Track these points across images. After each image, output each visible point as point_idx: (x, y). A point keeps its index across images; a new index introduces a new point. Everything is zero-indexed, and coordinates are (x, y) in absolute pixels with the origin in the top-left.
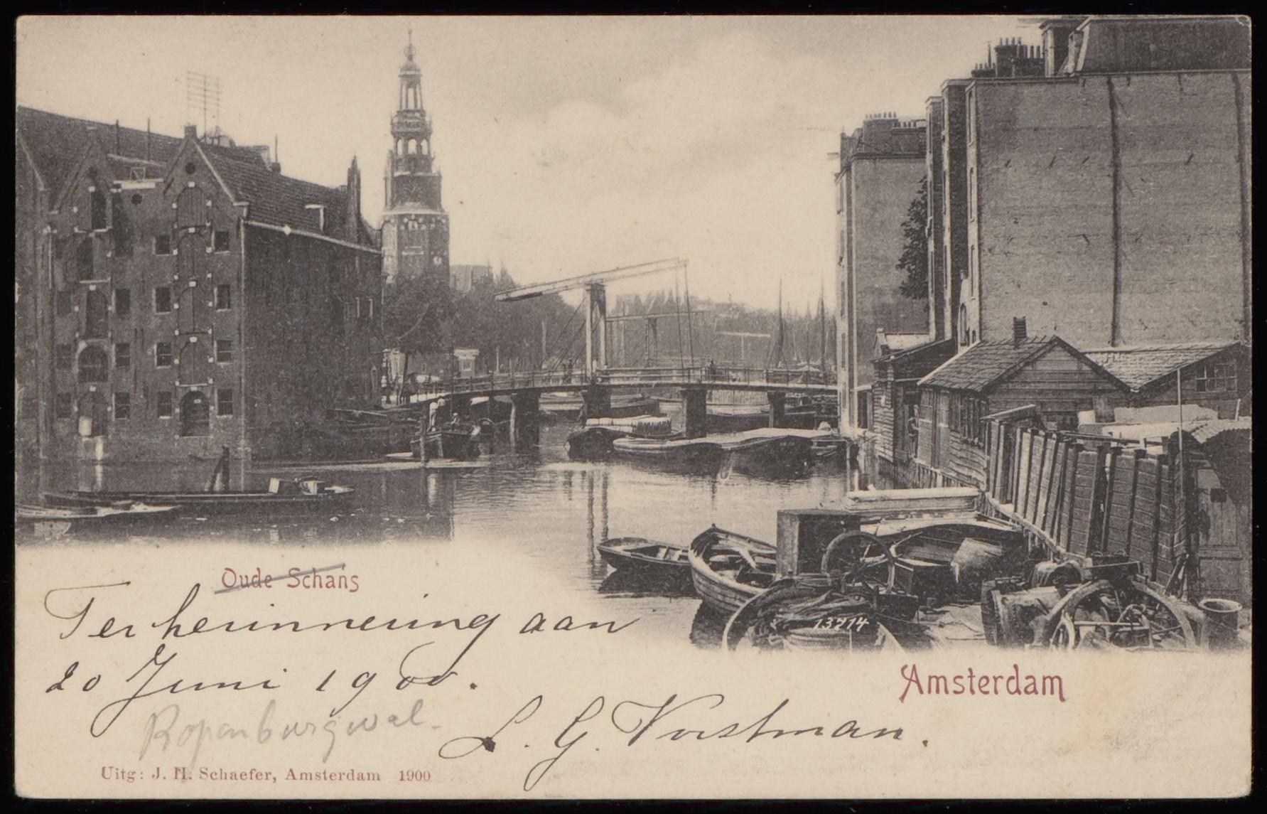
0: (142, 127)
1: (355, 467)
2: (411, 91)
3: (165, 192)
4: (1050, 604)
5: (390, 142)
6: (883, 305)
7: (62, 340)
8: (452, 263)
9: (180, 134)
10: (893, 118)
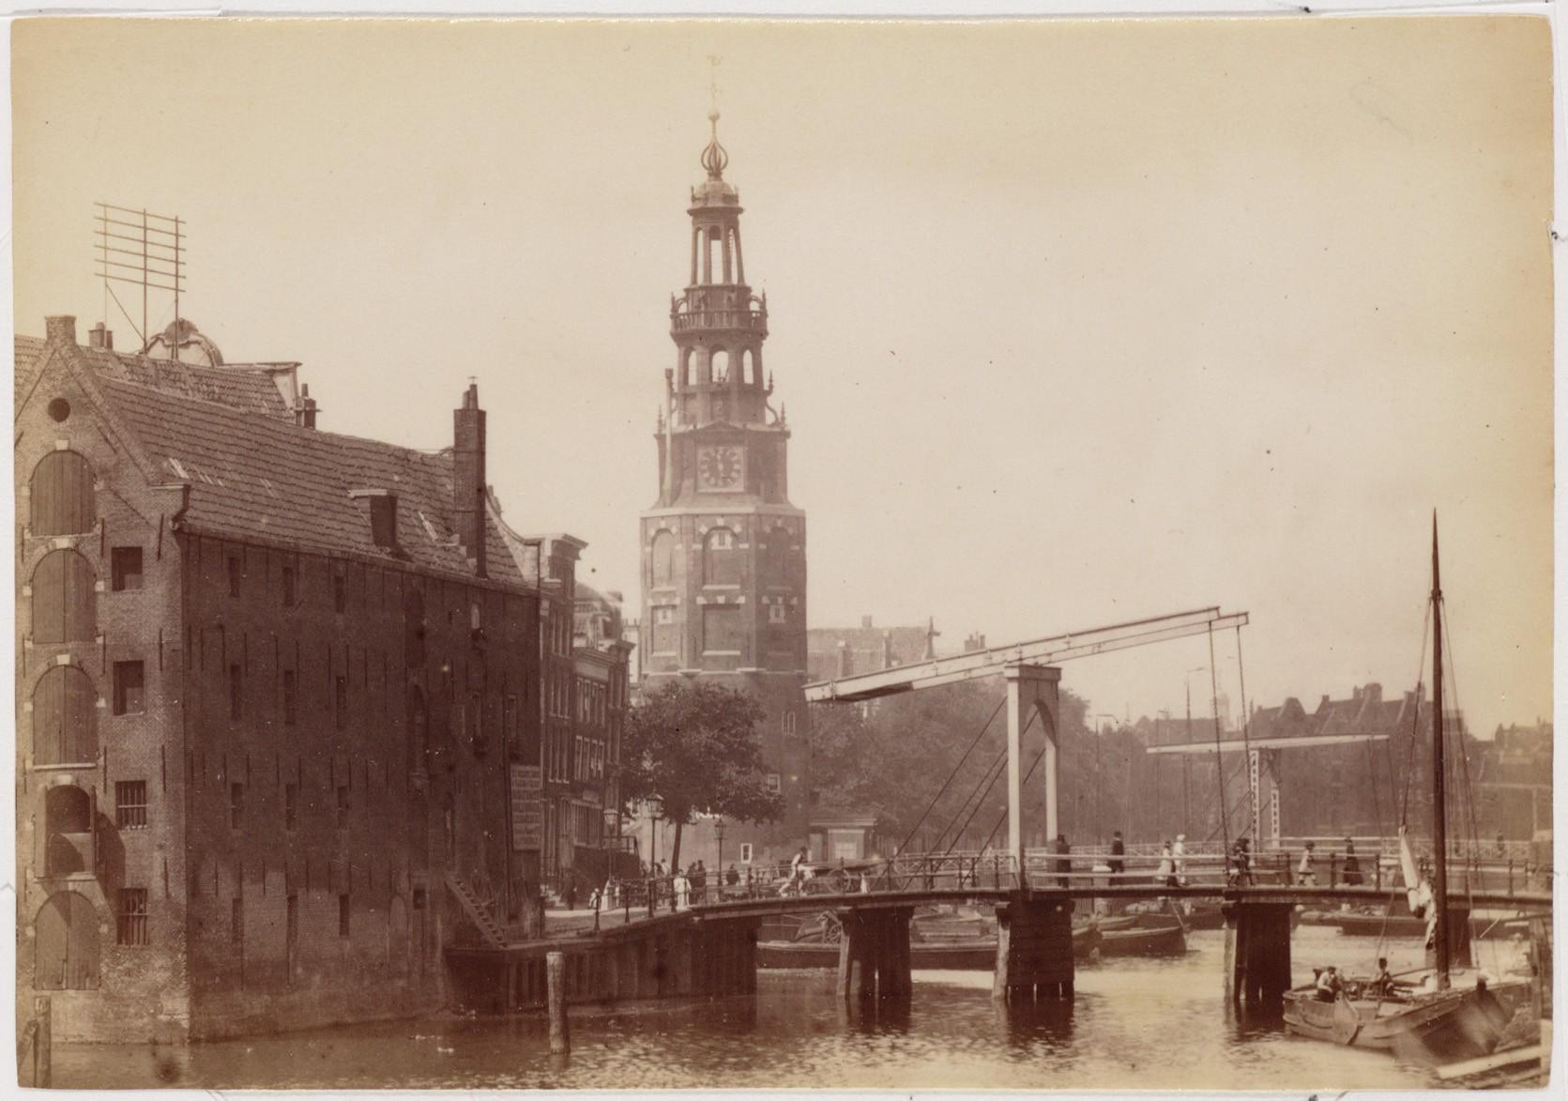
1: (1158, 930)
2: (717, 246)
5: (669, 354)
8: (812, 622)
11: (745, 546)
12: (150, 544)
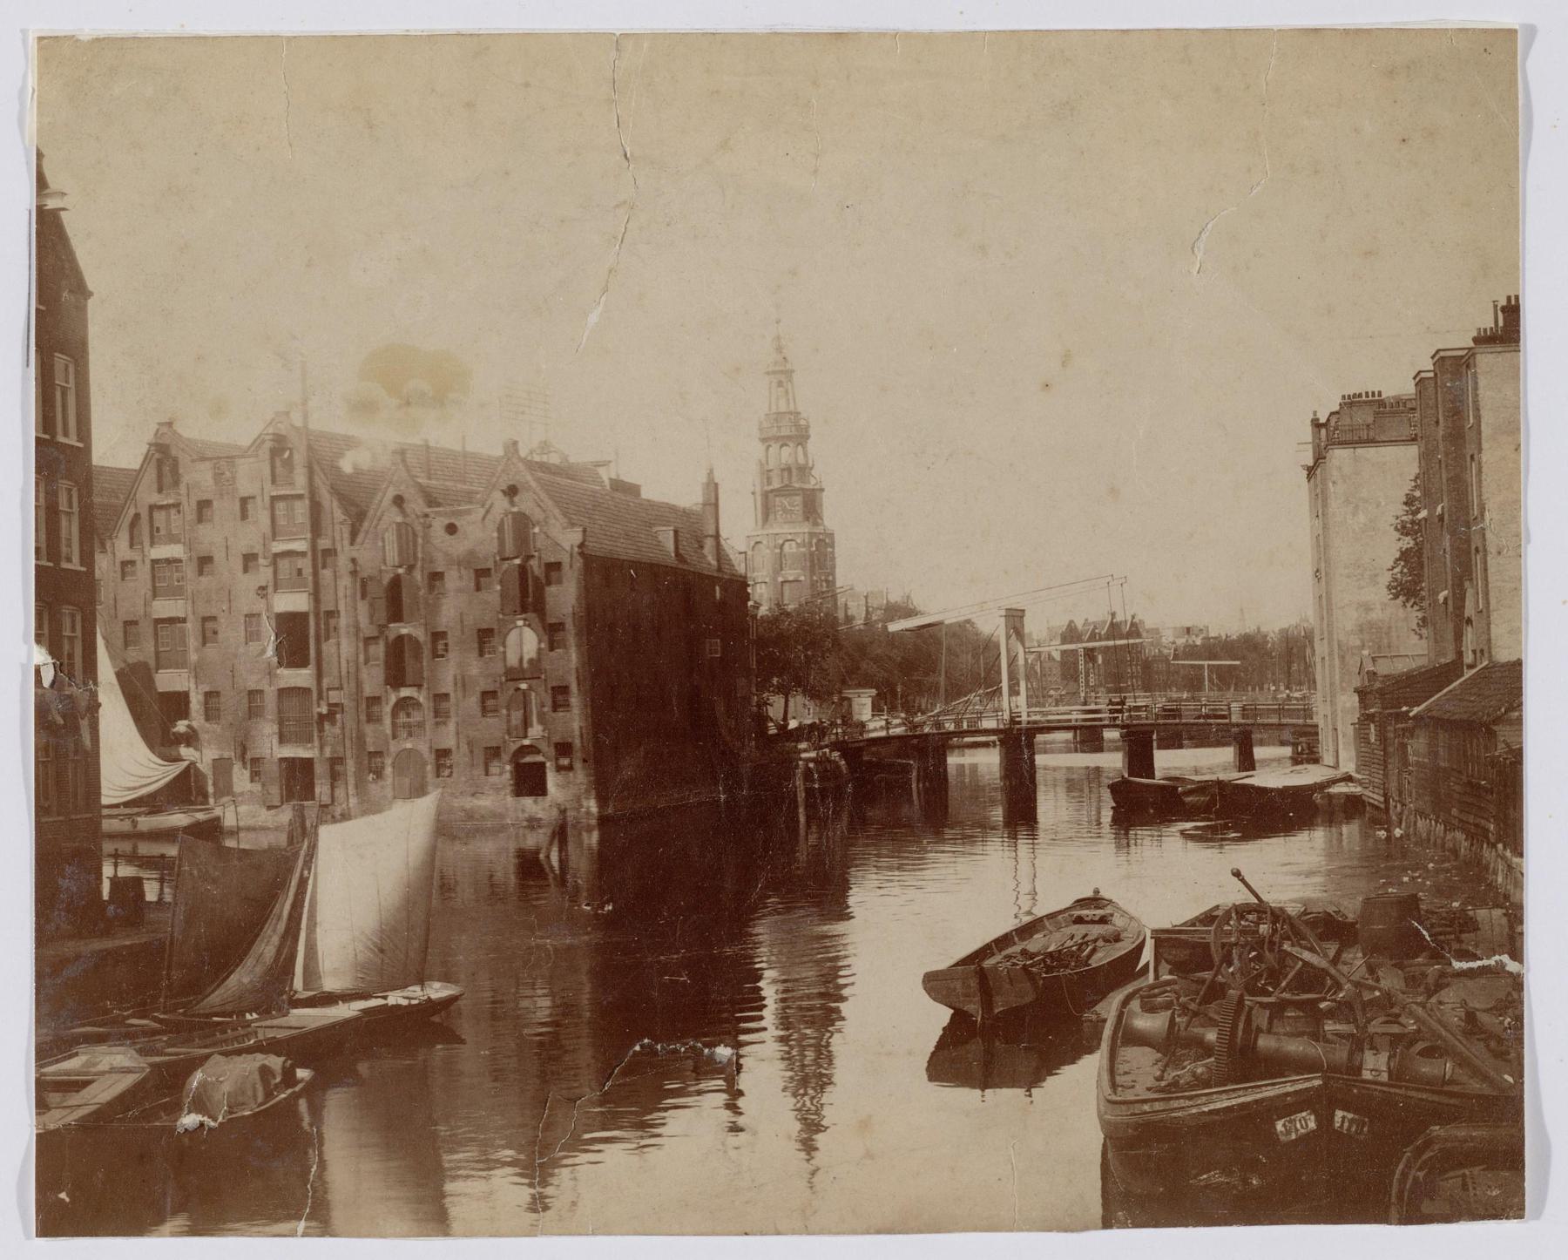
0: (457, 447)
3: (484, 518)
4: (1178, 834)
6: (1371, 624)
7: (368, 690)
9: (499, 452)
10: (1377, 398)
11: (803, 550)
12: (566, 560)
